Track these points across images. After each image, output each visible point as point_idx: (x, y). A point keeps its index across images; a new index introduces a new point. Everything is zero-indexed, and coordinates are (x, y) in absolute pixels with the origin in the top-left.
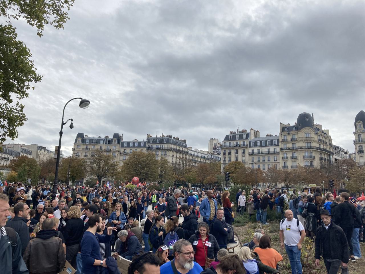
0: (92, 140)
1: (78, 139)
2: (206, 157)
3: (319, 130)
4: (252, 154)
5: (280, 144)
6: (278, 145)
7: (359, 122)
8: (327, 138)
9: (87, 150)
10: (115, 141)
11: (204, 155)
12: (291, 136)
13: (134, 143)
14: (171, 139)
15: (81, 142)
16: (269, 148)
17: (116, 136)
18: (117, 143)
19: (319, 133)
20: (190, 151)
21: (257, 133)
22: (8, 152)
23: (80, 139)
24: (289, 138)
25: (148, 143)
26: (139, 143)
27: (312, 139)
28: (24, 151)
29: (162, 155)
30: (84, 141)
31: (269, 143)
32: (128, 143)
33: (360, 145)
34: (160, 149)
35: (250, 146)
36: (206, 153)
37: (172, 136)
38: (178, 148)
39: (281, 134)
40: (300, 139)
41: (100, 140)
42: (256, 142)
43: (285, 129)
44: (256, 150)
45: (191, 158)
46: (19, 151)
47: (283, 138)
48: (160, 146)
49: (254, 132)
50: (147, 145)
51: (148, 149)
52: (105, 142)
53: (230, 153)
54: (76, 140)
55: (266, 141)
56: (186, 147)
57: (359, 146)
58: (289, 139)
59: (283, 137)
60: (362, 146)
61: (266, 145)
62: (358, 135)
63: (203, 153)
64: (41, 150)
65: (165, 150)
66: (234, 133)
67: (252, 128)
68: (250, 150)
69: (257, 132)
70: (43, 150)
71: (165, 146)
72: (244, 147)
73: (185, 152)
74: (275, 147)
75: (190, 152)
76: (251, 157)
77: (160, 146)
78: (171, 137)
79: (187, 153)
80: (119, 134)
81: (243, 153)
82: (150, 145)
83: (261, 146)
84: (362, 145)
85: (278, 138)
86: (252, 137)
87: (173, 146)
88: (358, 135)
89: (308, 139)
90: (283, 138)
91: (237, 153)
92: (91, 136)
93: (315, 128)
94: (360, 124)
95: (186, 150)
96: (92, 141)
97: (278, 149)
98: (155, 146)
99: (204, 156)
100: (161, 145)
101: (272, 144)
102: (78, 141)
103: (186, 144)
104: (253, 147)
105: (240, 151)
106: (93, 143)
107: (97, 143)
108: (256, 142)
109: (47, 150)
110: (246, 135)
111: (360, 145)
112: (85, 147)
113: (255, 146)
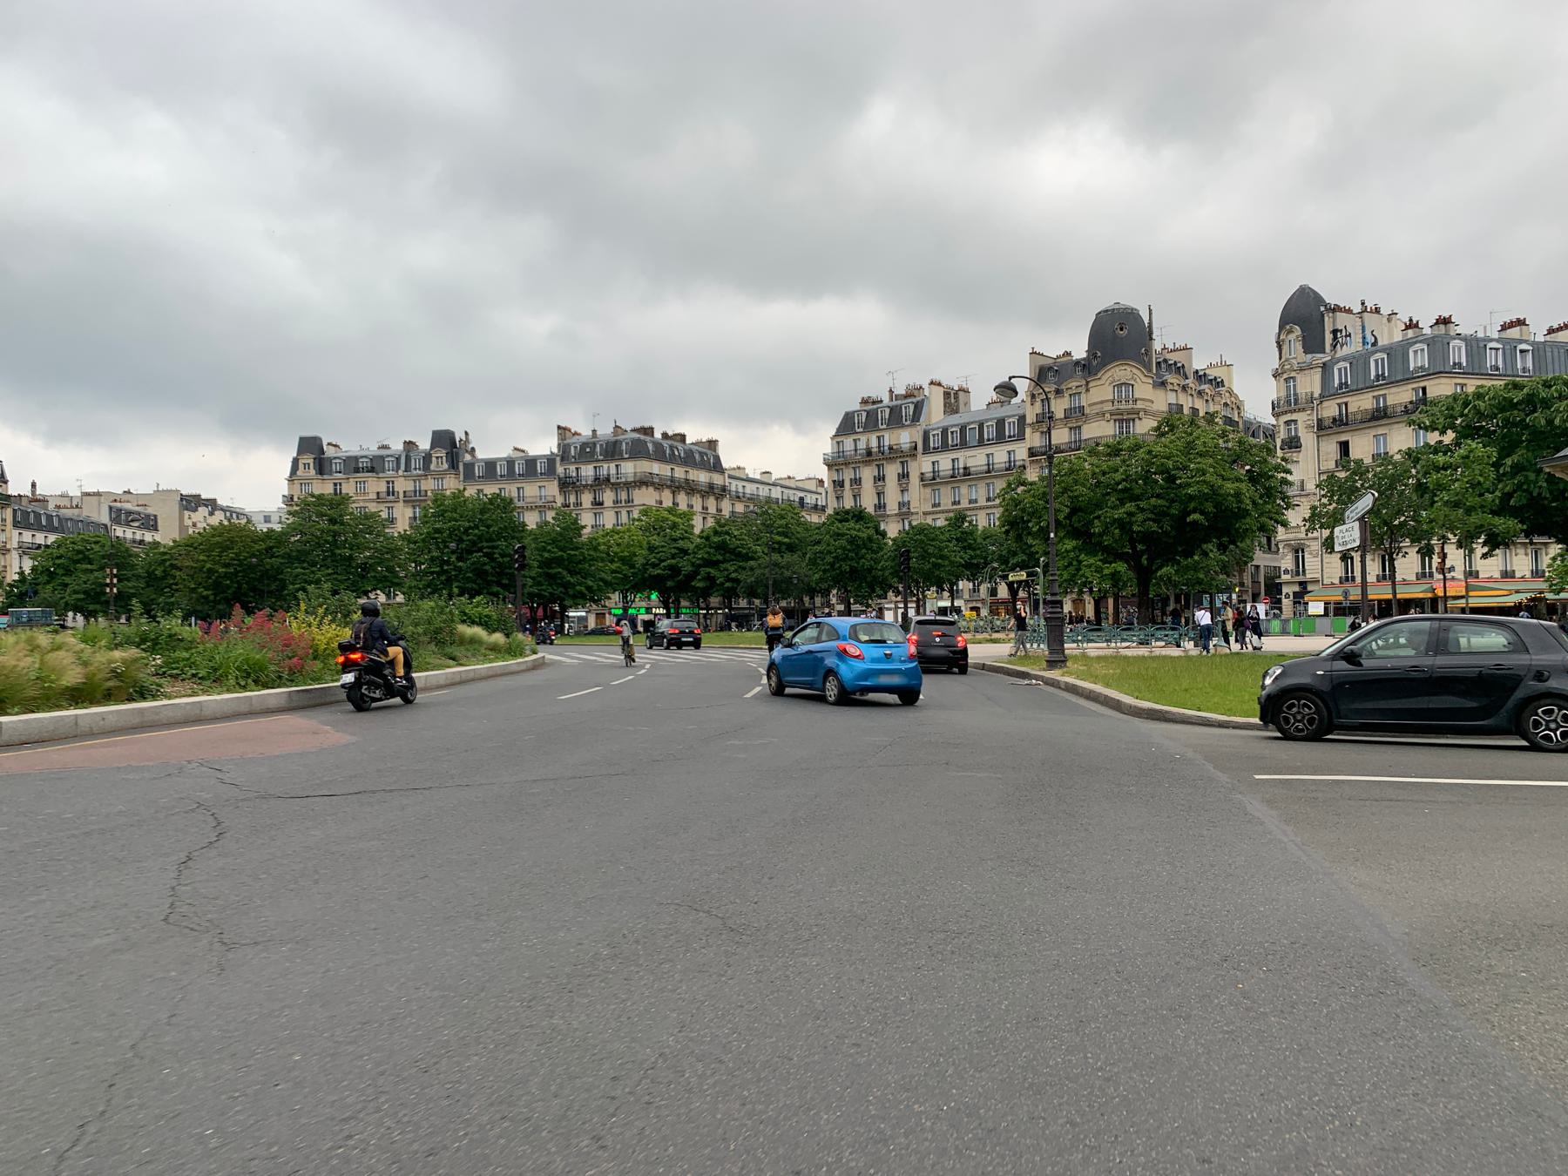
0: (356, 459)
1: (301, 463)
2: (808, 500)
3: (1179, 370)
4: (932, 481)
5: (1028, 431)
6: (1021, 437)
7: (1290, 332)
8: (1217, 399)
9: (391, 498)
10: (440, 462)
11: (802, 494)
12: (1067, 398)
13: (510, 463)
14: (648, 439)
15: (313, 472)
16: (989, 450)
17: (444, 440)
18: (446, 466)
19: (1175, 381)
20: (734, 483)
21: (956, 397)
22: (56, 524)
23: (308, 459)
24: (1059, 407)
25: (562, 460)
26: (531, 462)
27: (1140, 405)
28: (118, 516)
29: (616, 502)
30: (322, 466)
31: (990, 432)
32: (490, 465)
33: (1288, 417)
34: (608, 479)
35: (927, 450)
36: (812, 486)
37: (652, 429)
38: (679, 473)
39: (1033, 396)
40: (1097, 409)
41: (382, 458)
42: (1001, 423)
43: (1048, 374)
44: (945, 462)
45: (740, 508)
46: (105, 518)
47: (1039, 410)
48: (608, 468)
49: (947, 395)
50: (560, 470)
51: (566, 485)
52: (403, 467)
53: (857, 482)
54: (295, 462)
55: (981, 426)
56: (717, 467)
57: (1288, 423)
58: (1059, 414)
59: (1038, 404)
60: (1295, 421)
61: (981, 443)
62: (1286, 380)
63: (800, 485)
64: (195, 510)
65: (629, 486)
66: (874, 403)
67: (937, 378)
68: (924, 464)
69: (956, 394)
70: (203, 511)
71: (629, 469)
72: (902, 456)
73: (711, 486)
74: (1010, 447)
75: (734, 486)
76: (928, 490)
77: (608, 468)
78: (648, 431)
79: (721, 493)
80: (453, 433)
81: (904, 476)
82: (572, 468)
83: (964, 444)
84: (1294, 416)
85: (1021, 412)
86: (935, 414)
87: (657, 469)
88: (1286, 380)
89: (1123, 406)
90: (1038, 408)
91: (880, 478)
92: (350, 447)
93: (1158, 364)
94: (1292, 337)
95: (718, 479)
96: (353, 465)
97: (1021, 453)
98: (588, 471)
99: (802, 499)
100: (613, 466)
101: (1000, 438)
102: (301, 466)
103: (717, 458)
104: (955, 448)
105: (892, 471)
106: (357, 470)
107: (372, 470)
108: (1001, 423)
109: (223, 509)
110: (912, 407)
111: (1288, 417)
112: (383, 488)
113: (945, 447)
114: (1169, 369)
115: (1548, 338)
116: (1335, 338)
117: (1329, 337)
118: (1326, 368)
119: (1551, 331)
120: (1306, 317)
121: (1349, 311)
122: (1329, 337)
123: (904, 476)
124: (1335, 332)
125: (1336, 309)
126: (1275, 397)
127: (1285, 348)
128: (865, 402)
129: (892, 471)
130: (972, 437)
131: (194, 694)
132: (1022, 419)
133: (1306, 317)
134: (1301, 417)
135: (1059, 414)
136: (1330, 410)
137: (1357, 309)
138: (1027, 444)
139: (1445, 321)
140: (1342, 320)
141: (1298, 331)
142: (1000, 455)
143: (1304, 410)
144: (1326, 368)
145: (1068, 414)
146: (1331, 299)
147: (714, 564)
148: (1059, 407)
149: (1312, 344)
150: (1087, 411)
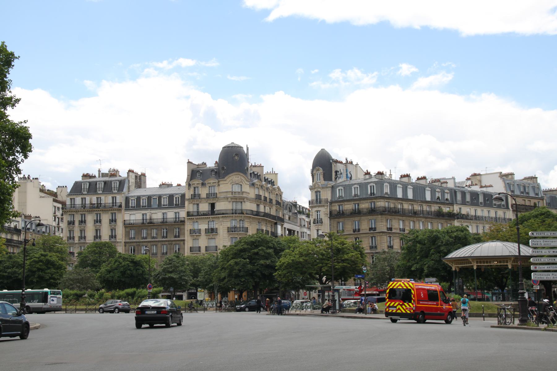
3: (258, 176)
5: (186, 203)
6: (182, 206)
12: (207, 188)
19: (258, 183)
21: (140, 179)
24: (203, 192)
27: (245, 195)
40: (223, 196)
43: (196, 173)
47: (192, 193)
49: (136, 177)
55: (96, 184)
58: (204, 195)
59: (192, 189)
60: (320, 211)
84: (319, 209)
91: (98, 221)
93: (251, 174)
97: (183, 214)
104: (144, 208)
114: (257, 176)
115: (417, 182)
116: (336, 175)
117: (334, 174)
118: (333, 188)
119: (418, 179)
120: (324, 165)
121: (341, 163)
122: (334, 174)
123: (113, 221)
124: (336, 172)
125: (337, 162)
126: (310, 199)
127: (315, 177)
128: (85, 176)
129: (106, 218)
130: (154, 203)
131: (501, 265)
132: (183, 196)
133: (324, 165)
134: (323, 209)
135: (204, 195)
136: (336, 208)
137: (344, 162)
138: (186, 209)
139: (380, 174)
140: (340, 167)
141: (321, 170)
142: (170, 215)
143: (324, 206)
144: (333, 188)
145: (208, 196)
146: (334, 157)
147: (42, 270)
148: (203, 192)
149: (327, 176)
150: (218, 196)
